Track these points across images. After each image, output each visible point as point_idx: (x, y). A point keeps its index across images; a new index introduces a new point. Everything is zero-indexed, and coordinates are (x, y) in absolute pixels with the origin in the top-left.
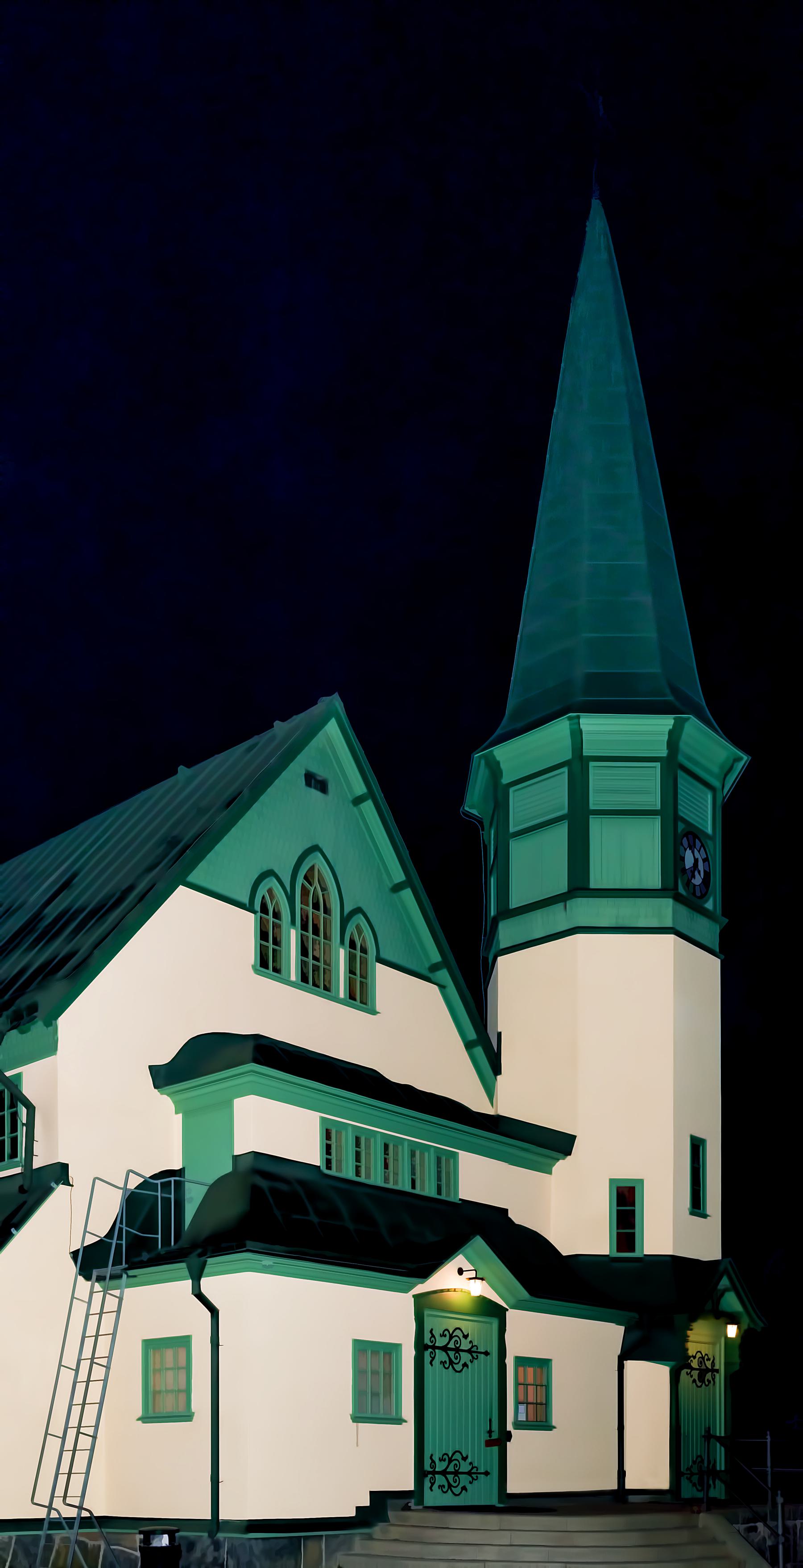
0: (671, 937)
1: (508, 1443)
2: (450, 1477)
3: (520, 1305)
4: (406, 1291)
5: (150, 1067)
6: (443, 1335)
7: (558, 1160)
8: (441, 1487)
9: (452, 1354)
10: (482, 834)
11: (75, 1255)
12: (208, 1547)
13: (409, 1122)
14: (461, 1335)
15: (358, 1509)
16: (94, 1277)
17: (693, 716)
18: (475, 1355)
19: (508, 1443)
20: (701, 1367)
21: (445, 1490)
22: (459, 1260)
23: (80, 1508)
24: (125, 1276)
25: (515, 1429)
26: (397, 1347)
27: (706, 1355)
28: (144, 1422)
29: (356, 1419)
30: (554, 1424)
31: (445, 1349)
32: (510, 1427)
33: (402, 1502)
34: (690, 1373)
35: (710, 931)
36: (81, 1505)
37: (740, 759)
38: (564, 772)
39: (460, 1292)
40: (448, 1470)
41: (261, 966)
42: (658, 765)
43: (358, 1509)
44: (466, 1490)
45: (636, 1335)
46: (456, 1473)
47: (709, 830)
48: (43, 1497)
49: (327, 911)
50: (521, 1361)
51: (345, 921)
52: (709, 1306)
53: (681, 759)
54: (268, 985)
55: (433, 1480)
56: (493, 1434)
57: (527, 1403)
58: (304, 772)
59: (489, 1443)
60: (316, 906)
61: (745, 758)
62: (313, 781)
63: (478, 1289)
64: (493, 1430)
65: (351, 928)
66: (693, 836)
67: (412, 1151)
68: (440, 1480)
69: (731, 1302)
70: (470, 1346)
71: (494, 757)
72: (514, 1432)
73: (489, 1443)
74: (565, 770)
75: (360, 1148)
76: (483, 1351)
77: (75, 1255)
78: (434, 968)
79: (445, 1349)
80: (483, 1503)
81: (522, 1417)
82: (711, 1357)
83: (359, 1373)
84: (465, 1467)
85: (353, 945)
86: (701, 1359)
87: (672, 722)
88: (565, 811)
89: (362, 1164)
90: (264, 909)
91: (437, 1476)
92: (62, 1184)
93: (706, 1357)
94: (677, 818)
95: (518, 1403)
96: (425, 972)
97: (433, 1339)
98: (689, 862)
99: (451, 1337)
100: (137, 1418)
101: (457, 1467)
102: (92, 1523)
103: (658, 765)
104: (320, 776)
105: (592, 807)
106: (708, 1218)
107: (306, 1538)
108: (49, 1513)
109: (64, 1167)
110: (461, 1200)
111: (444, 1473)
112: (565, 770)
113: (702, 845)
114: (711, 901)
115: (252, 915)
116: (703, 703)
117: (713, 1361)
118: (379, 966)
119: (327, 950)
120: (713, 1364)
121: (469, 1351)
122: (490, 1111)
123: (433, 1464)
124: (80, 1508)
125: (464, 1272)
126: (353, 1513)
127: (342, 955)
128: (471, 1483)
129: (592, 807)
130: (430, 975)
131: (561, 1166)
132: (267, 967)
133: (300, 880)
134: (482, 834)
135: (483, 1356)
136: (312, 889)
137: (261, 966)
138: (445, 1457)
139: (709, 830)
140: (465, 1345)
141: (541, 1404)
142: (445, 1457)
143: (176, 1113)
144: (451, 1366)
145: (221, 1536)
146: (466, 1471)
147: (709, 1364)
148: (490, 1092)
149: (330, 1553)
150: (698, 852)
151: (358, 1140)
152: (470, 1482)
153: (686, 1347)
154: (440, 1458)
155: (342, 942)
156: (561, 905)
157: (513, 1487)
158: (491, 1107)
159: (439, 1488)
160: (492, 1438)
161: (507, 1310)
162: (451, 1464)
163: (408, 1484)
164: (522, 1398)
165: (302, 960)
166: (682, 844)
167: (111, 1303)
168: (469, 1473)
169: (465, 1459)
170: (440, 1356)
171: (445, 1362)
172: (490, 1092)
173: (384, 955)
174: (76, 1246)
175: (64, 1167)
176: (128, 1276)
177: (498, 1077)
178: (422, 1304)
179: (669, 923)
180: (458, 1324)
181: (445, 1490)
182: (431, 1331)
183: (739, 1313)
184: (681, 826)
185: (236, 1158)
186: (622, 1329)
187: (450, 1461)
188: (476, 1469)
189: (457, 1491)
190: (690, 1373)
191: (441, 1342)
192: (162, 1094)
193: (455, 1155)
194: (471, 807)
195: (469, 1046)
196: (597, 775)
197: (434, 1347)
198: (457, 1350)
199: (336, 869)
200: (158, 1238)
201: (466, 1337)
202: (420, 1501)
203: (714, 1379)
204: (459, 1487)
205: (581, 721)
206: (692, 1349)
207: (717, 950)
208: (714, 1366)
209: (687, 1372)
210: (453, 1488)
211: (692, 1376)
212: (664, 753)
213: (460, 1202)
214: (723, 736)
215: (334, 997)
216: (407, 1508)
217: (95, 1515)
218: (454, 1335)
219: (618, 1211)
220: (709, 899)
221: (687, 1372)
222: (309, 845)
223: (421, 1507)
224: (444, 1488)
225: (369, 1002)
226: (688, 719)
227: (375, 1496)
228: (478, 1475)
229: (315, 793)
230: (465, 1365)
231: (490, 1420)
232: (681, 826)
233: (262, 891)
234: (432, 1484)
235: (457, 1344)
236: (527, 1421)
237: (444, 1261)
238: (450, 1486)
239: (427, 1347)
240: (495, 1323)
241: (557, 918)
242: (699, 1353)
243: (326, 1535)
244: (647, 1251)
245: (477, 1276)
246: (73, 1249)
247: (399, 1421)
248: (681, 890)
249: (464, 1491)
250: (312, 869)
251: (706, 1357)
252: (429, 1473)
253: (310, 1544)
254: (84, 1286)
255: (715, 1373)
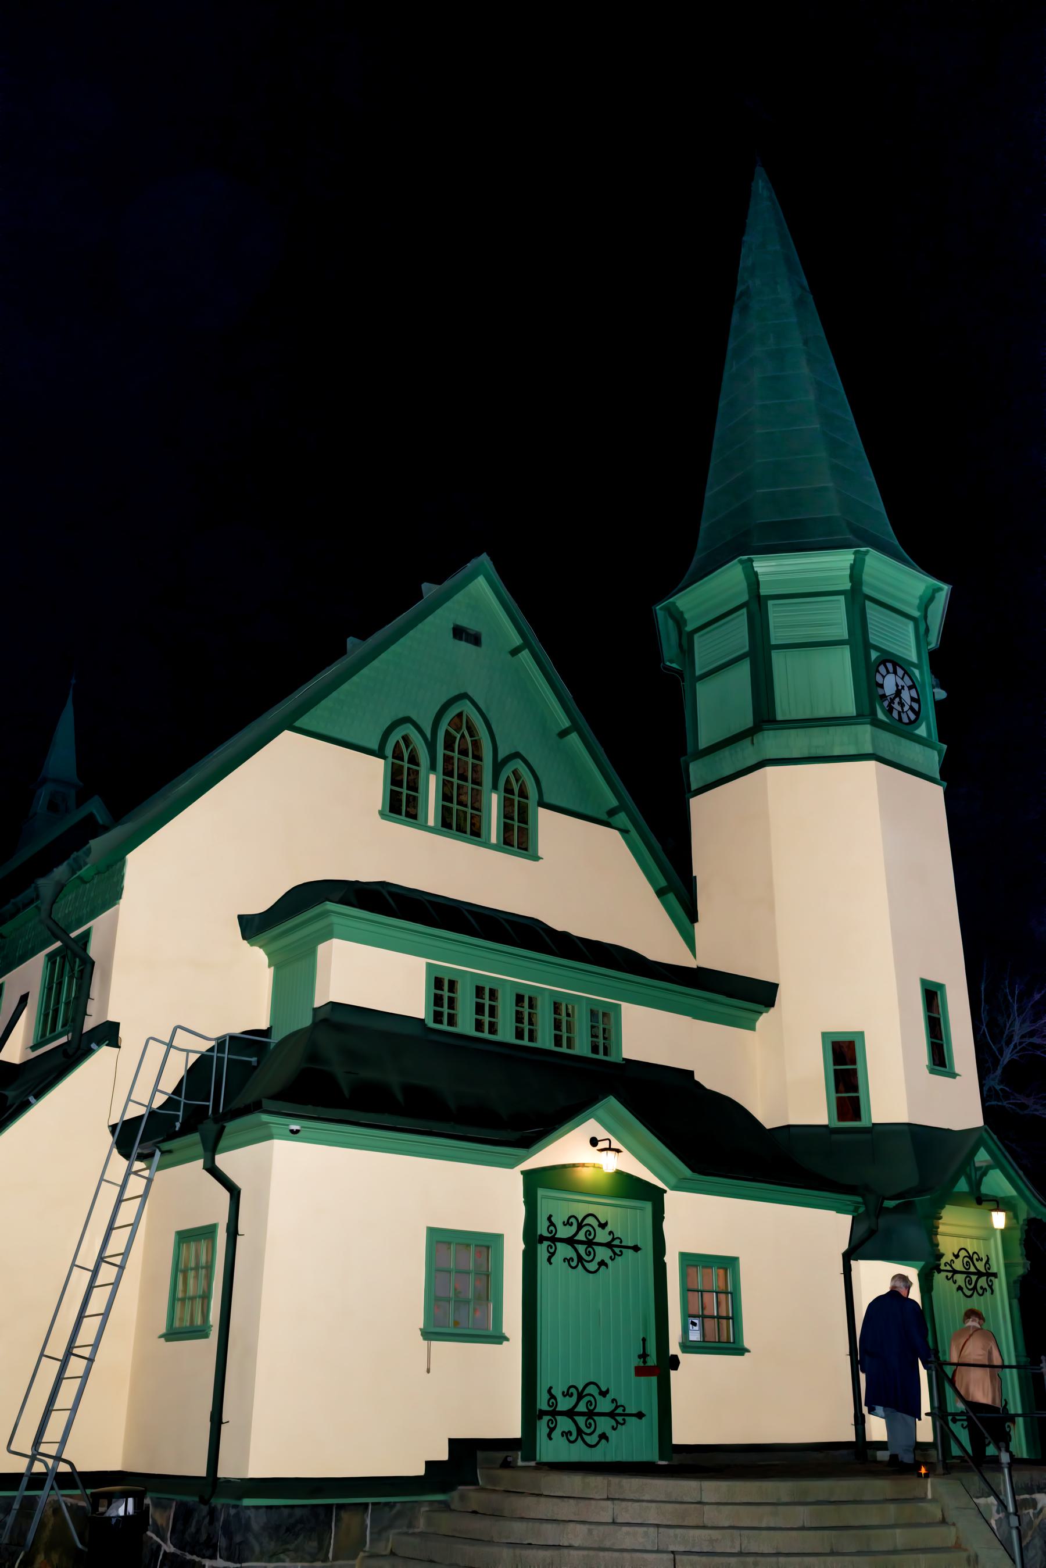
0: (872, 764)
1: (672, 1373)
2: (581, 1420)
3: (680, 1186)
4: (511, 1166)
5: (241, 918)
6: (568, 1223)
7: (761, 1013)
8: (566, 1434)
9: (581, 1249)
10: (683, 685)
11: (113, 1128)
12: (204, 1518)
13: (463, 949)
14: (595, 1224)
15: (429, 1464)
16: (134, 1154)
17: (872, 548)
18: (617, 1250)
19: (672, 1373)
20: (969, 1268)
21: (572, 1438)
22: (591, 1127)
23: (58, 1458)
24: (158, 1153)
25: (683, 1352)
26: (498, 1238)
27: (975, 1253)
28: (167, 1340)
29: (428, 1335)
30: (746, 1345)
31: (571, 1241)
32: (674, 1349)
33: (500, 1455)
34: (952, 1277)
35: (932, 759)
36: (58, 1456)
37: (940, 589)
38: (743, 614)
39: (592, 1168)
40: (577, 1410)
41: (443, 826)
42: (842, 598)
43: (429, 1464)
44: (607, 1439)
45: (863, 1228)
46: (591, 1414)
47: (914, 658)
48: (24, 1442)
49: (478, 757)
50: (688, 1260)
51: (498, 767)
52: (962, 1185)
53: (866, 590)
54: (400, 832)
55: (552, 1423)
56: (648, 1359)
57: (703, 1317)
58: (452, 626)
59: (640, 1371)
60: (464, 752)
61: (946, 588)
62: (464, 635)
63: (611, 1163)
64: (648, 1352)
65: (507, 772)
66: (893, 662)
67: (555, 1003)
68: (564, 1424)
69: (997, 1183)
70: (610, 1238)
71: (677, 609)
72: (682, 1357)
73: (640, 1371)
74: (744, 611)
75: (454, 993)
76: (630, 1244)
77: (113, 1128)
78: (612, 813)
79: (571, 1241)
80: (636, 1458)
81: (695, 1335)
82: (983, 1256)
83: (436, 1270)
84: (604, 1405)
85: (509, 790)
86: (966, 1259)
87: (852, 557)
88: (747, 649)
89: (575, 1034)
90: (397, 755)
91: (558, 1418)
92: (107, 1045)
93: (975, 1256)
94: (868, 646)
95: (688, 1317)
96: (604, 817)
97: (552, 1228)
98: (889, 688)
99: (580, 1226)
100: (159, 1335)
101: (591, 1405)
102: (74, 1480)
103: (842, 598)
104: (472, 630)
105: (773, 642)
106: (958, 1077)
107: (341, 1507)
108: (31, 1465)
109: (115, 1026)
110: (624, 1059)
111: (571, 1414)
112: (744, 611)
113: (906, 672)
114: (923, 727)
115: (382, 761)
116: (897, 543)
117: (987, 1262)
118: (542, 812)
119: (477, 795)
120: (987, 1266)
121: (609, 1245)
122: (690, 963)
123: (553, 1400)
124: (58, 1458)
125: (599, 1143)
126: (421, 1471)
127: (494, 802)
128: (614, 1429)
129: (773, 642)
130: (610, 820)
131: (765, 1020)
132: (449, 827)
133: (444, 726)
134: (683, 685)
135: (630, 1251)
136: (458, 736)
137: (443, 826)
138: (572, 1390)
139: (914, 658)
140: (602, 1236)
141: (727, 1318)
142: (572, 1390)
143: (269, 966)
144: (580, 1264)
145: (218, 1502)
146: (607, 1410)
147: (981, 1266)
148: (690, 942)
149: (379, 1533)
150: (901, 680)
151: (557, 1008)
152: (613, 1427)
153: (935, 1242)
154: (563, 1393)
155: (495, 787)
156: (748, 741)
157: (682, 1435)
158: (694, 960)
159: (563, 1436)
160: (646, 1365)
161: (665, 1191)
162: (581, 1402)
163: (514, 1430)
164: (696, 1309)
165: (443, 806)
166: (878, 671)
167: (136, 1186)
168: (612, 1415)
169: (604, 1394)
170: (564, 1250)
171: (572, 1259)
172: (690, 942)
173: (547, 799)
174: (116, 1119)
175: (115, 1026)
176: (163, 1153)
177: (696, 925)
178: (534, 1180)
179: (868, 749)
180: (592, 1209)
181: (572, 1438)
182: (549, 1218)
183: (1013, 1197)
184: (874, 655)
185: (315, 1010)
186: (848, 1218)
187: (580, 1397)
188: (622, 1408)
189: (592, 1440)
190: (952, 1277)
191: (564, 1232)
192: (251, 945)
193: (619, 1006)
194: (672, 662)
195: (660, 893)
196: (775, 613)
197: (554, 1240)
198: (590, 1243)
199: (490, 716)
200: (209, 1106)
201: (603, 1226)
202: (530, 1455)
203: (991, 1287)
204: (595, 1434)
205: (755, 564)
206: (948, 1245)
207: (938, 776)
208: (989, 1269)
209: (947, 1277)
210: (585, 1437)
211: (955, 1282)
212: (847, 586)
213: (624, 1062)
214: (922, 571)
215: (485, 843)
216: (506, 1465)
217: (79, 1469)
218: (584, 1223)
219: (835, 1071)
220: (920, 725)
221: (947, 1277)
222: (457, 693)
223: (533, 1464)
224: (571, 1435)
225: (530, 848)
226: (867, 552)
227: (454, 1444)
228: (626, 1418)
229: (464, 646)
230: (602, 1263)
231: (644, 1340)
232: (874, 655)
233: (396, 736)
234: (552, 1430)
235: (590, 1235)
236: (704, 1341)
237: (557, 1126)
238: (580, 1432)
239: (542, 1239)
240: (648, 1206)
241: (746, 753)
242: (975, 1255)
243: (373, 1504)
244: (876, 1119)
245: (612, 1147)
246: (111, 1123)
247: (499, 1338)
248: (881, 715)
249: (603, 1441)
250: (460, 715)
251: (975, 1256)
252: (546, 1413)
253: (345, 1515)
254: (119, 1164)
255: (993, 1278)
